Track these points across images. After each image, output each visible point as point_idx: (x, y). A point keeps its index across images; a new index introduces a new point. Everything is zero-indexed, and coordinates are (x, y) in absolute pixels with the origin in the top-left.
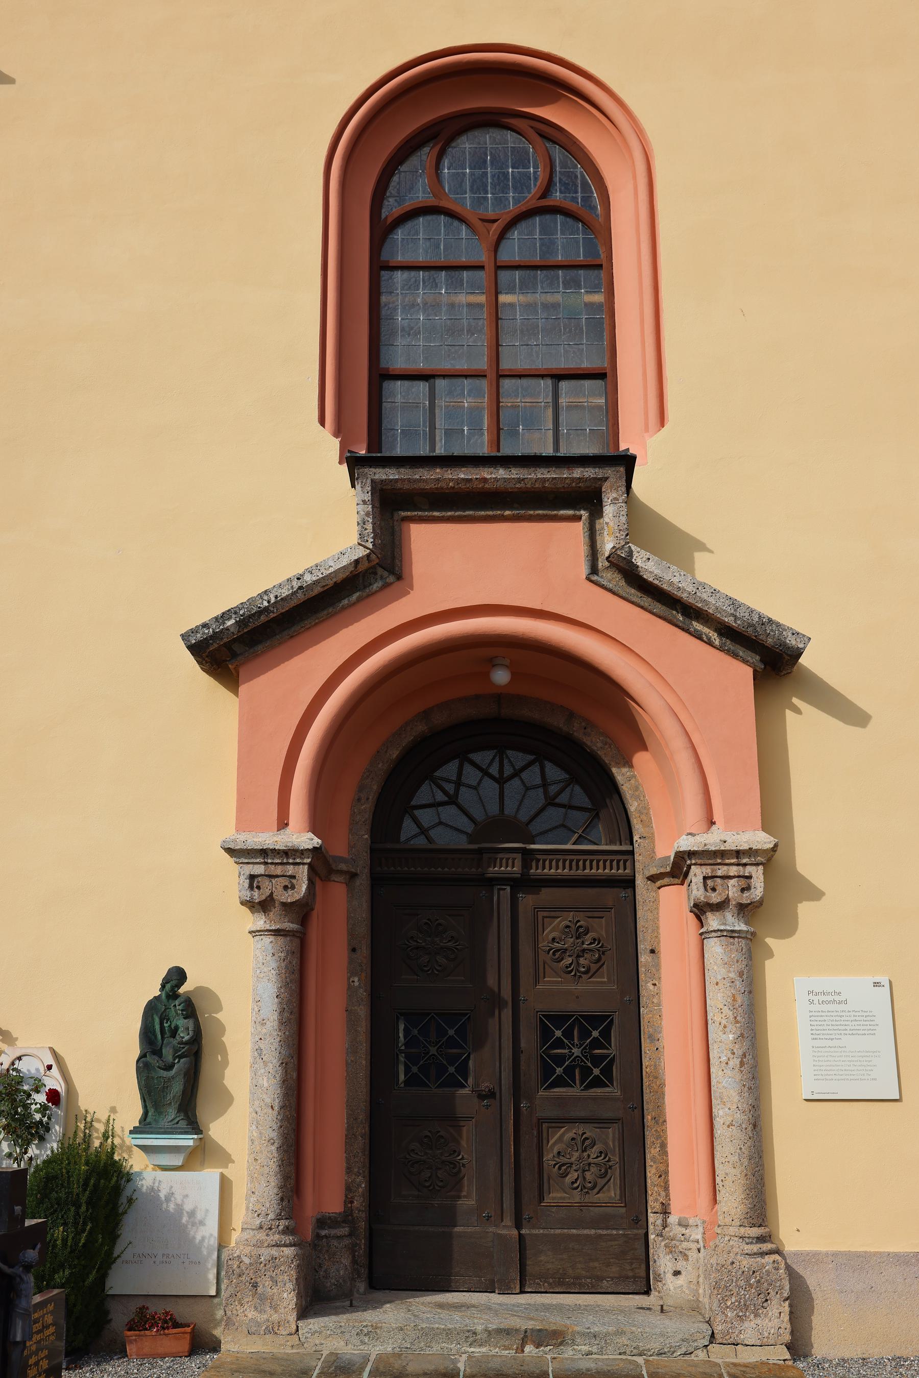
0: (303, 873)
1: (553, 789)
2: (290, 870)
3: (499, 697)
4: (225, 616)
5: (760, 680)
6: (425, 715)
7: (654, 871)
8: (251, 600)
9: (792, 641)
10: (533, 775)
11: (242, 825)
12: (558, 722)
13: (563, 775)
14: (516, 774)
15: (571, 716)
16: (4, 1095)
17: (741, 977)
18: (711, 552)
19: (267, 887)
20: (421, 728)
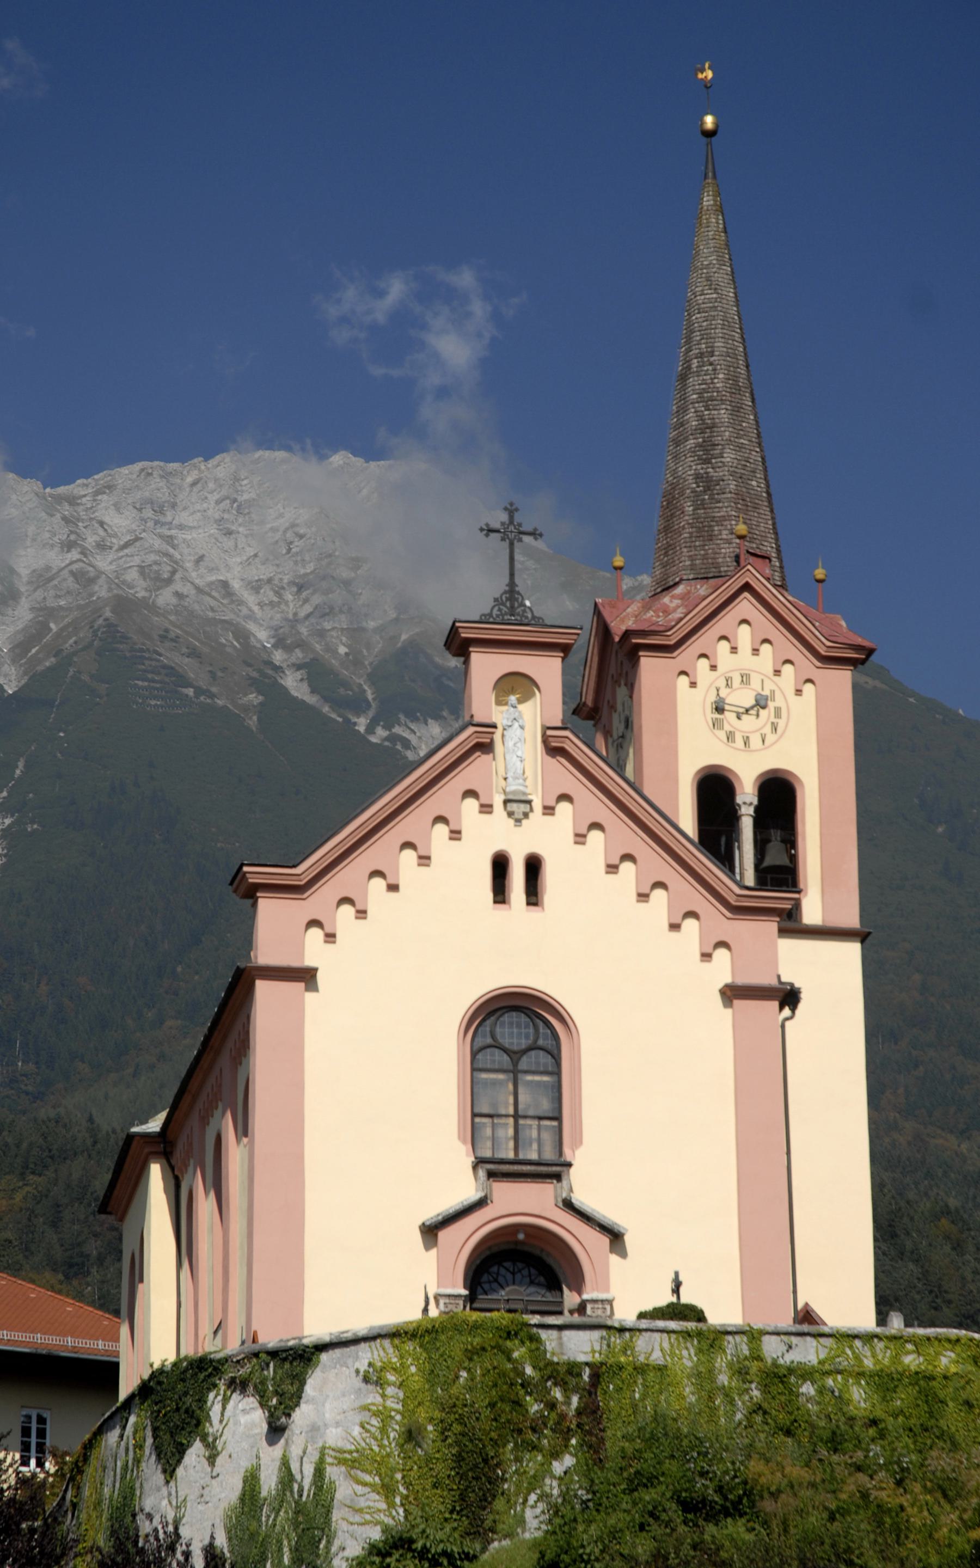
0: (461, 1303)
1: (491, 1278)
2: (457, 1302)
3: (517, 1242)
4: (438, 1215)
5: (611, 1242)
6: (490, 1248)
7: (572, 1307)
8: (447, 1210)
9: (622, 1231)
10: (525, 1272)
11: (438, 1287)
12: (537, 1252)
13: (537, 1272)
14: (520, 1271)
15: (542, 1250)
16: (163, 1427)
17: (460, 1434)
18: (677, 1274)
19: (450, 1307)
20: (488, 1253)
